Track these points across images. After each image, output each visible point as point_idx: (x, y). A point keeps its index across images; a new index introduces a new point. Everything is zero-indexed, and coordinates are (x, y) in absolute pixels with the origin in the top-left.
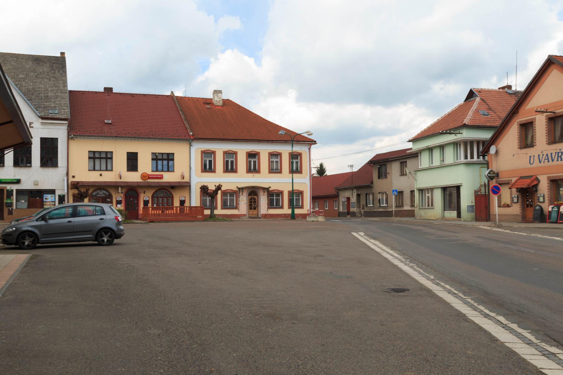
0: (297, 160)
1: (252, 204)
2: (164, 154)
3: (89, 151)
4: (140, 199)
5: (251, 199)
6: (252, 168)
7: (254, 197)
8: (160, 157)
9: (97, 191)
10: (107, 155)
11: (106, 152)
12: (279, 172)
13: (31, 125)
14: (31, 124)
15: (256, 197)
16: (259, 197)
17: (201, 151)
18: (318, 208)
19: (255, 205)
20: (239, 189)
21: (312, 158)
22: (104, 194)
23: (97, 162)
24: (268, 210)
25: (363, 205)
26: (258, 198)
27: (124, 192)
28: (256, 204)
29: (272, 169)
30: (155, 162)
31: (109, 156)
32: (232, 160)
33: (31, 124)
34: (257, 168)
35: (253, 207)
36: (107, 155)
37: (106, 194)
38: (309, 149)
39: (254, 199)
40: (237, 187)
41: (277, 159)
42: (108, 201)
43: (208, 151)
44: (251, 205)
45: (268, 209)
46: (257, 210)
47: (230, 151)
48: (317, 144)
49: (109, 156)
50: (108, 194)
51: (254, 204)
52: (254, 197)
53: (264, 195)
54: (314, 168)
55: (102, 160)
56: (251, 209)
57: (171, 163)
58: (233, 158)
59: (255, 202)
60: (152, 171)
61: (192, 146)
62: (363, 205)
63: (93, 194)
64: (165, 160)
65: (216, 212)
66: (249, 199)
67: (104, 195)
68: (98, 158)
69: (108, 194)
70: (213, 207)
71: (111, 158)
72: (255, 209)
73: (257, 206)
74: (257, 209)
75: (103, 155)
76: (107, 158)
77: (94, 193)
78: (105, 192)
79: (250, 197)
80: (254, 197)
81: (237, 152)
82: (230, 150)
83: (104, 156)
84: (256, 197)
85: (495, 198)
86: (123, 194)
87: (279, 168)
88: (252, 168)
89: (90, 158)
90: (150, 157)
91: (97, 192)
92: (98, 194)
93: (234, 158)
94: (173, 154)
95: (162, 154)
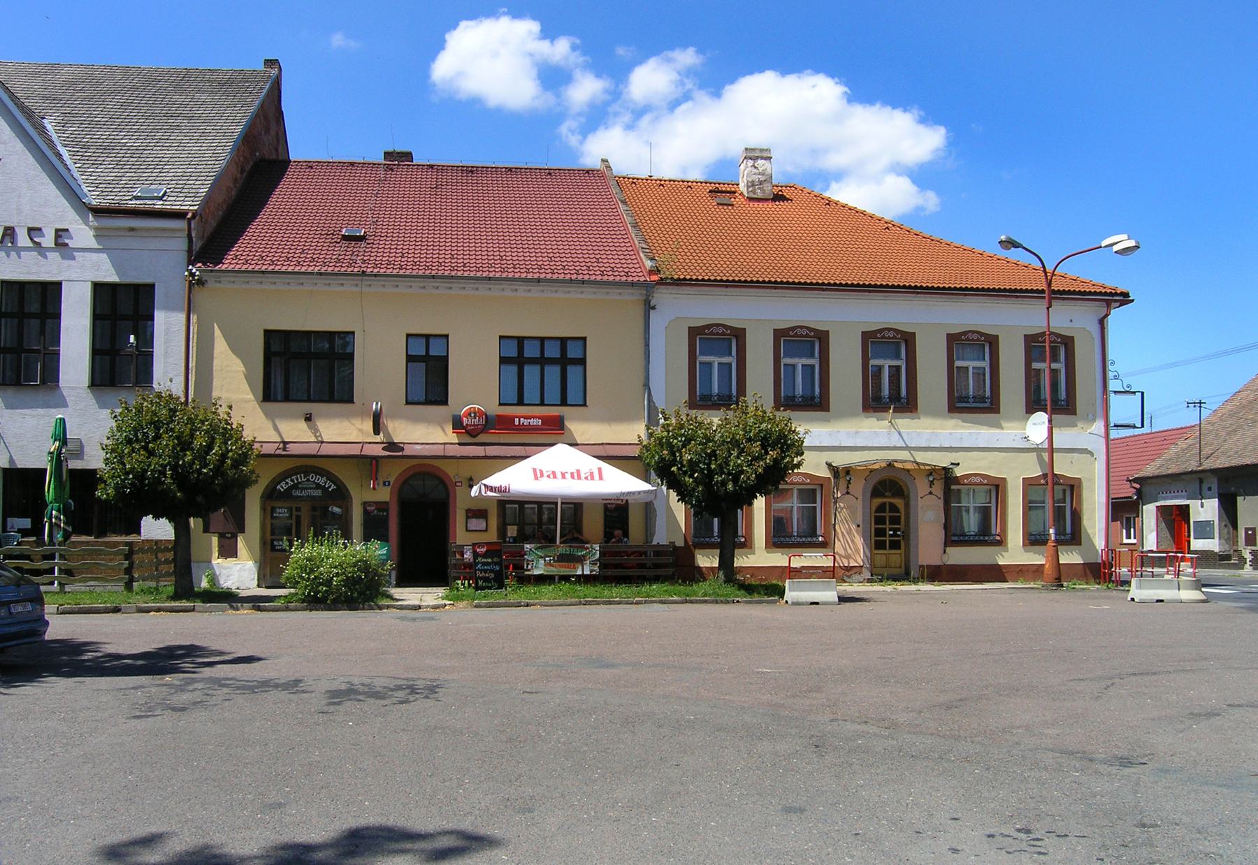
0: (726, 360)
1: (885, 529)
2: (432, 341)
3: (501, 337)
4: (455, 506)
5: (881, 508)
6: (886, 391)
7: (890, 503)
8: (531, 351)
9: (294, 477)
10: (564, 349)
11: (563, 341)
12: (986, 408)
13: (60, 236)
14: (60, 233)
15: (899, 502)
16: (912, 503)
17: (948, 334)
18: (1135, 538)
19: (895, 530)
20: (835, 471)
21: (1111, 355)
22: (318, 486)
23: (531, 372)
24: (948, 549)
25: (1247, 530)
26: (907, 506)
27: (392, 480)
28: (899, 529)
29: (964, 399)
30: (513, 369)
31: (573, 352)
32: (726, 360)
33: (60, 233)
34: (903, 393)
35: (887, 539)
36: (564, 349)
37: (325, 489)
38: (1102, 323)
39: (894, 508)
40: (829, 465)
41: (978, 359)
42: (333, 514)
43: (799, 331)
44: (880, 533)
45: (946, 545)
46: (902, 551)
47: (801, 327)
48: (1133, 301)
49: (573, 352)
50: (333, 487)
51: (890, 530)
52: (892, 500)
53: (931, 493)
54: (1115, 392)
55: (548, 369)
56: (879, 545)
57: (573, 371)
58: (730, 354)
59: (895, 520)
60: (500, 404)
61: (654, 308)
62: (1247, 530)
63: (278, 487)
64: (552, 361)
65: (742, 560)
66: (874, 508)
67: (318, 493)
68: (532, 361)
69: (333, 487)
70: (731, 542)
71: (582, 362)
72: (895, 545)
73: (906, 536)
74: (902, 544)
75: (552, 351)
76: (564, 362)
77: (283, 484)
78: (322, 481)
79: (878, 501)
80: (892, 500)
81: (997, 336)
82: (886, 329)
83: (570, 355)
84: (899, 502)
85: (66, 476)
86: (389, 488)
87: (988, 393)
88: (886, 391)
89: (504, 361)
90: (492, 354)
91: (292, 481)
92: (295, 487)
93: (817, 354)
94: (581, 343)
95: (542, 340)
